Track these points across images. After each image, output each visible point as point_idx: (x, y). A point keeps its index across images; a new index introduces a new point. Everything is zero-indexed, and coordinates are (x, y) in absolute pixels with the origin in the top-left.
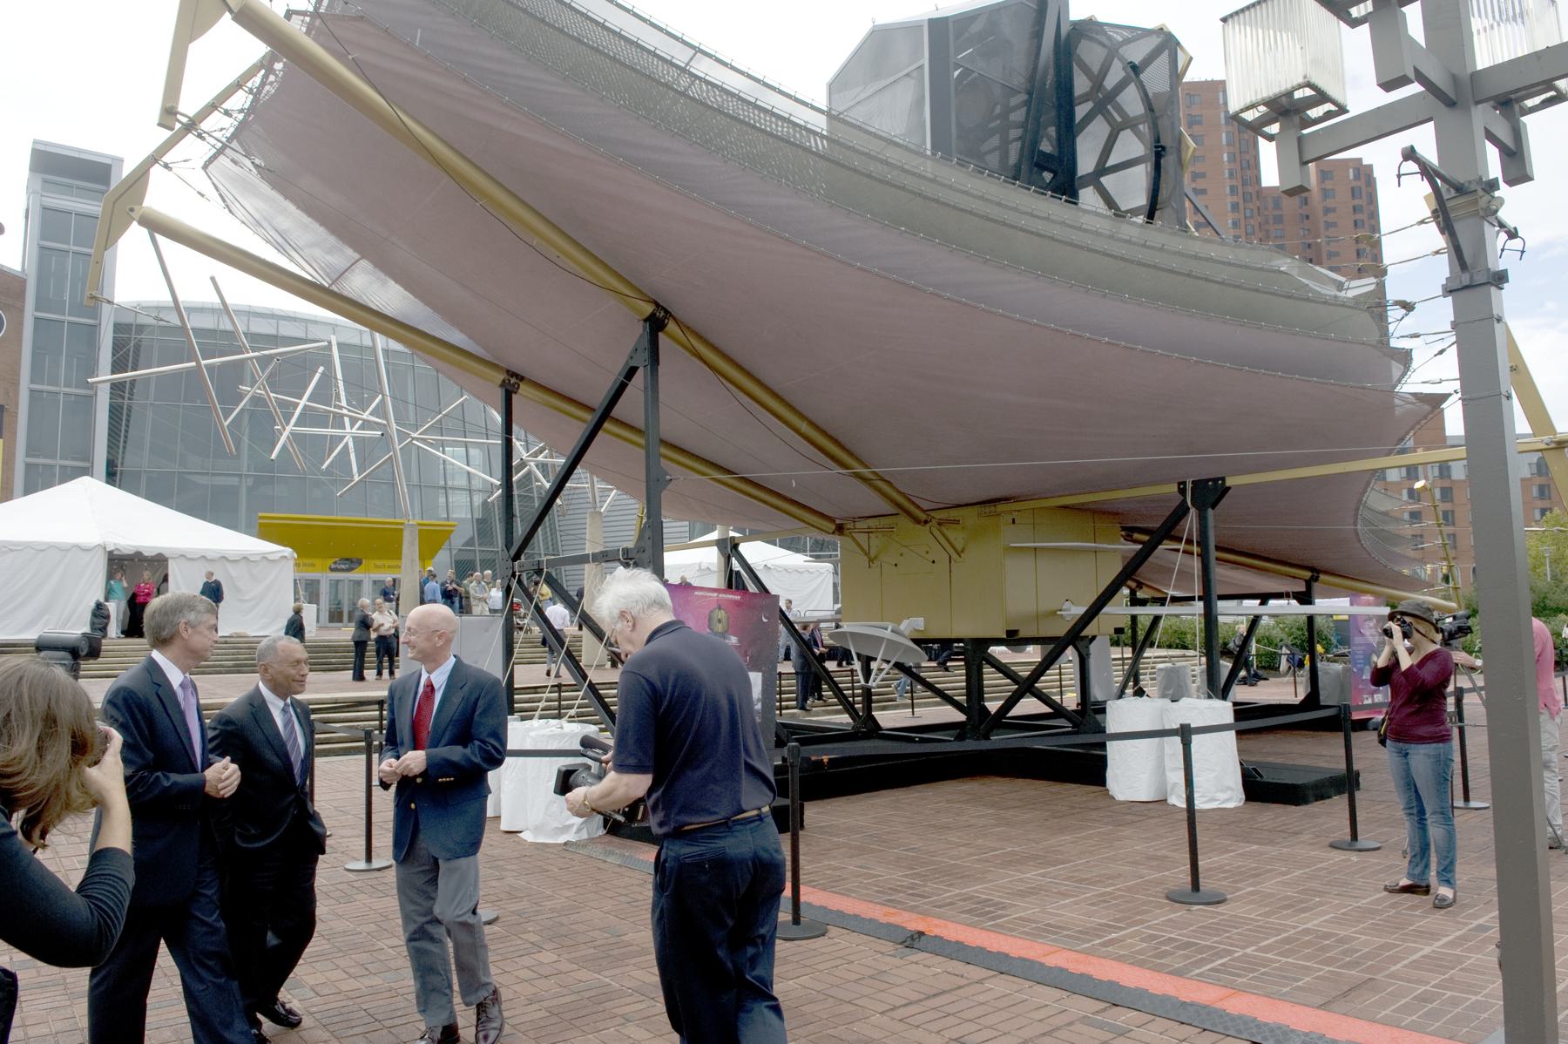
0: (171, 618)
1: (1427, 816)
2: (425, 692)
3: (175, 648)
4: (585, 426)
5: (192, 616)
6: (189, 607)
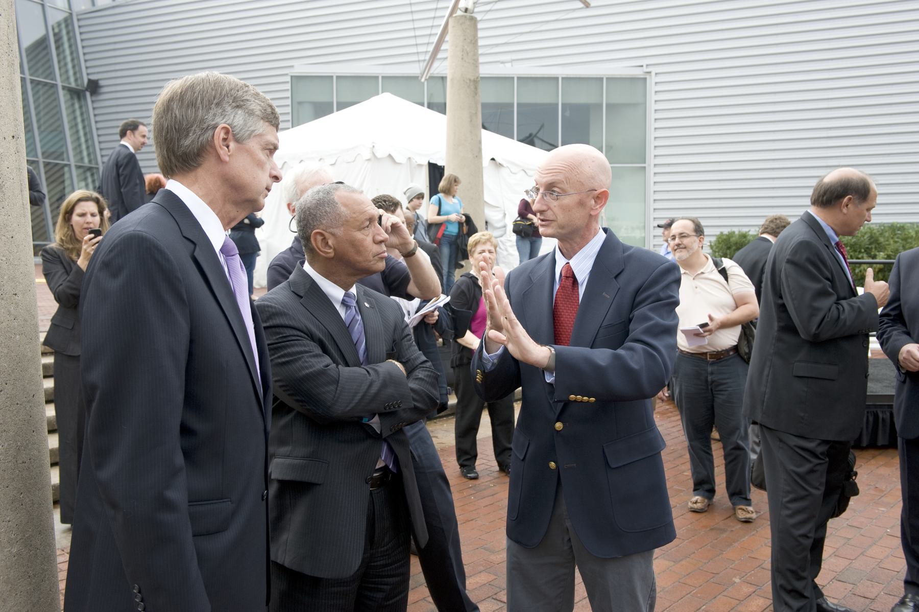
1: (430, 387)
2: (562, 287)
3: (206, 173)
5: (238, 119)
6: (235, 99)
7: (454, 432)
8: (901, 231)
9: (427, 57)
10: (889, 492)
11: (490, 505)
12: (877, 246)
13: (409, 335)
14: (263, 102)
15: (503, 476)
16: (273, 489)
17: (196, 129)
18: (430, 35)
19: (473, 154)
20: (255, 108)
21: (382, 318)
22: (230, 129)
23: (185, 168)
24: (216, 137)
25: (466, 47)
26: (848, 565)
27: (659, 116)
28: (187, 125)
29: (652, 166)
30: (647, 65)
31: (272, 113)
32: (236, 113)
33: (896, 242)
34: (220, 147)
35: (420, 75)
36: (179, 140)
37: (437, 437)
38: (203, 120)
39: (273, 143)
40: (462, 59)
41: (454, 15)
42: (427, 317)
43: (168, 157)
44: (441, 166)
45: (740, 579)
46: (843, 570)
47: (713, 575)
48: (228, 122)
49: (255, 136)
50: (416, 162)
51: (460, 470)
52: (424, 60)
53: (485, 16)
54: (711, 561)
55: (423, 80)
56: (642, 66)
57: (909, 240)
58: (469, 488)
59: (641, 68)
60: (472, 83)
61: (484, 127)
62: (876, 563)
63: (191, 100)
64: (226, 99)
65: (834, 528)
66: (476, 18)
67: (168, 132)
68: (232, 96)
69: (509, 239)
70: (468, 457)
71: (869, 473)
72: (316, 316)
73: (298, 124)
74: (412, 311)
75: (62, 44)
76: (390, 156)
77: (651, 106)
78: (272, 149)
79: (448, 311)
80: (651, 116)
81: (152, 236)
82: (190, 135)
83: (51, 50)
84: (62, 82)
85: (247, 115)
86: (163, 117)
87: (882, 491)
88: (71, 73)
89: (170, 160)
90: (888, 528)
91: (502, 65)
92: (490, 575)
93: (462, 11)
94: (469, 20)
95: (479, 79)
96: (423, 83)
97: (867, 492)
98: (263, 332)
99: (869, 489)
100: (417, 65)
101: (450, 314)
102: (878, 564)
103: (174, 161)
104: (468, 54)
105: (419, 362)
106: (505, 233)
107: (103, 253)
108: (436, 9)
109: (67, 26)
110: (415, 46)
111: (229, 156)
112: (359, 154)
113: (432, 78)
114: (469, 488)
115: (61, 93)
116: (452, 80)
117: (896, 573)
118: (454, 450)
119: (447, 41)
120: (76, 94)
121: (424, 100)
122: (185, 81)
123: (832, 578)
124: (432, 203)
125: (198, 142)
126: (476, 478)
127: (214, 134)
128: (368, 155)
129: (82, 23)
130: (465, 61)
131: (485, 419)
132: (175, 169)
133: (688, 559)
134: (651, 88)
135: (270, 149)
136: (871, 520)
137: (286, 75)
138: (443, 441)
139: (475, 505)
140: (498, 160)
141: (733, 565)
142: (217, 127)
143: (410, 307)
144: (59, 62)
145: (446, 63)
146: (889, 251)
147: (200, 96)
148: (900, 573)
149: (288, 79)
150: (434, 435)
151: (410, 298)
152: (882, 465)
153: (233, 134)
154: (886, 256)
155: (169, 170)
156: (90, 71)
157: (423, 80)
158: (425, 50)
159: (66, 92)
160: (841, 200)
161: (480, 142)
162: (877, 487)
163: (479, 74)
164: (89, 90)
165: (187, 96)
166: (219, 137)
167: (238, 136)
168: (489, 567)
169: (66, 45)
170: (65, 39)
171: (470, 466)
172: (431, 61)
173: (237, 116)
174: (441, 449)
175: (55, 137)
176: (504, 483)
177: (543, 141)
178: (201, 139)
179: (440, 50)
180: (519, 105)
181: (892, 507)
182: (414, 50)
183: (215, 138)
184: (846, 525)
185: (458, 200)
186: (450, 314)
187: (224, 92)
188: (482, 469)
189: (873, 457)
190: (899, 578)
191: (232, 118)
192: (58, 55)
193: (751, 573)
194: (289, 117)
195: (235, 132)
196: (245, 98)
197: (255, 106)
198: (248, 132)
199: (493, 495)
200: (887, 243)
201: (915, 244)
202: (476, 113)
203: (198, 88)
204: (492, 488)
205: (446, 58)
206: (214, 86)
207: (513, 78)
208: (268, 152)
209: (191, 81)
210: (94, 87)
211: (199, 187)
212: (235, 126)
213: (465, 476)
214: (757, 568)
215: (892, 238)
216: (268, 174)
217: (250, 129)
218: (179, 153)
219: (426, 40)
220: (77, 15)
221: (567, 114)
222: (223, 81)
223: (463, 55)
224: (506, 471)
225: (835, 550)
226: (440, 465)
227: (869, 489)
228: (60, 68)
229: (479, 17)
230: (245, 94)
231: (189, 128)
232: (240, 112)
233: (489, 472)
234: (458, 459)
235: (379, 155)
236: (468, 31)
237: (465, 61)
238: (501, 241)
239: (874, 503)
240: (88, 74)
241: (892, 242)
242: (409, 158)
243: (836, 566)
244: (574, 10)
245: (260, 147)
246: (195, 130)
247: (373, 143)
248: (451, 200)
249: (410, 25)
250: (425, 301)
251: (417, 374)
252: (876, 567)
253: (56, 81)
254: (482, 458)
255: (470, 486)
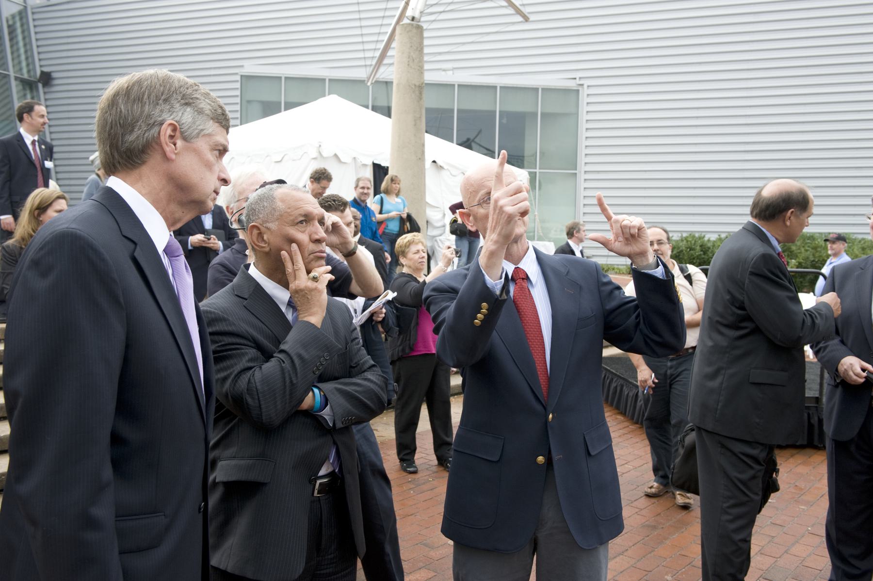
0: (147, 108)
4: (750, 207)
5: (186, 116)
6: (184, 97)
7: (394, 425)
8: (811, 240)
9: (374, 62)
10: (808, 490)
11: (429, 499)
12: (790, 254)
13: (357, 338)
14: (214, 102)
15: (442, 470)
16: (214, 499)
17: (142, 124)
18: (377, 41)
19: (417, 157)
20: (204, 106)
21: (330, 318)
22: (178, 126)
23: (128, 165)
24: (162, 133)
25: (412, 54)
26: (773, 564)
27: (590, 125)
28: (132, 120)
29: (583, 172)
30: (580, 78)
31: (223, 114)
32: (185, 111)
33: (807, 251)
34: (167, 144)
35: (366, 79)
36: (123, 135)
37: (377, 430)
38: (150, 115)
39: (222, 143)
40: (408, 65)
41: (401, 23)
42: (375, 315)
43: (111, 154)
44: (384, 167)
45: (672, 577)
46: (769, 568)
47: (647, 572)
48: (176, 119)
49: (204, 135)
50: (361, 162)
51: (399, 464)
52: (371, 65)
53: (430, 25)
54: (643, 558)
55: (369, 84)
56: (575, 79)
57: (819, 249)
58: (409, 482)
59: (574, 80)
60: (417, 89)
61: (426, 132)
62: (800, 561)
63: (138, 95)
64: (174, 95)
65: (759, 526)
66: (422, 27)
67: (112, 127)
68: (181, 93)
69: (448, 238)
70: (409, 451)
71: (788, 472)
72: (263, 321)
73: (247, 122)
74: (359, 310)
75: (16, 36)
76: (336, 155)
77: (583, 117)
78: (223, 151)
79: (392, 309)
80: (583, 125)
81: (87, 234)
82: (136, 130)
83: (4, 42)
84: (14, 73)
85: (196, 113)
86: (107, 112)
87: (801, 489)
88: (24, 64)
89: (113, 157)
90: (809, 527)
91: (443, 73)
92: (430, 571)
93: (409, 19)
94: (416, 28)
95: (424, 85)
96: (369, 87)
97: (788, 490)
98: (209, 338)
99: (789, 487)
100: (363, 69)
101: (395, 312)
102: (801, 563)
103: (116, 157)
104: (413, 60)
105: (368, 366)
106: (444, 232)
107: (33, 251)
108: (383, 17)
109: (21, 19)
110: (363, 52)
111: (176, 154)
112: (305, 153)
113: (377, 82)
114: (409, 482)
115: (14, 83)
116: (398, 84)
117: (819, 571)
118: (394, 443)
119: (394, 48)
120: (29, 85)
121: (368, 103)
122: (132, 77)
123: (759, 576)
124: (374, 203)
125: (143, 138)
126: (415, 472)
127: (160, 131)
128: (315, 154)
129: (36, 16)
130: (411, 67)
131: (424, 412)
132: (118, 165)
133: (621, 556)
134: (584, 99)
135: (219, 150)
136: (793, 518)
137: (236, 74)
138: (383, 434)
139: (414, 499)
140: (439, 162)
141: (665, 563)
142: (163, 124)
143: (356, 305)
144: (12, 53)
145: (391, 69)
146: (801, 258)
147: (147, 91)
148: (822, 572)
149: (238, 78)
150: (375, 428)
151: (353, 297)
152: (800, 464)
153: (181, 132)
154: (797, 264)
155: (111, 167)
156: (43, 63)
157: (369, 84)
158: (372, 55)
159: (18, 82)
160: (784, 214)
161: (423, 145)
162: (796, 486)
163: (424, 80)
164: (42, 81)
165: (134, 91)
166: (165, 134)
167: (186, 134)
168: (428, 563)
169: (20, 37)
170: (19, 31)
171: (410, 460)
172: (376, 68)
173: (186, 114)
174: (381, 443)
175: (7, 125)
176: (443, 477)
177: (481, 146)
178: (146, 135)
179: (386, 56)
180: (458, 110)
181: (812, 506)
182: (361, 55)
183: (161, 134)
184: (770, 523)
185: (402, 200)
186: (395, 312)
187: (173, 89)
188: (421, 463)
189: (792, 456)
190: (821, 577)
191: (180, 115)
192: (12, 46)
193: (682, 571)
194: (238, 115)
195: (182, 130)
196: (195, 96)
197: (205, 105)
198: (197, 131)
199: (431, 490)
200: (799, 251)
201: (824, 253)
202: (420, 117)
203: (146, 83)
204: (431, 482)
205: (392, 64)
206: (163, 82)
207: (454, 85)
208: (217, 153)
209: (138, 77)
210: (46, 79)
211: (142, 186)
212: (183, 124)
213: (405, 470)
214: (687, 565)
215: (803, 247)
216: (216, 177)
217: (199, 128)
218: (122, 149)
219: (372, 46)
220: (32, 9)
221: (504, 121)
222: (172, 78)
223: (409, 62)
224: (445, 465)
225: (761, 548)
226: (380, 460)
227: (789, 487)
228: (13, 59)
229: (425, 26)
230: (195, 92)
231: (134, 123)
232: (189, 109)
233: (428, 466)
234: (399, 454)
235: (325, 154)
236: (415, 39)
237: (411, 67)
238: (440, 240)
239: (795, 501)
240: (41, 66)
241: (803, 250)
242: (355, 158)
243: (762, 564)
244: (513, 23)
245: (208, 147)
246: (140, 126)
247: (320, 142)
248: (394, 200)
249: (358, 32)
250: (371, 299)
251: (366, 375)
252: (800, 565)
253: (8, 71)
254: (421, 452)
255: (410, 480)
